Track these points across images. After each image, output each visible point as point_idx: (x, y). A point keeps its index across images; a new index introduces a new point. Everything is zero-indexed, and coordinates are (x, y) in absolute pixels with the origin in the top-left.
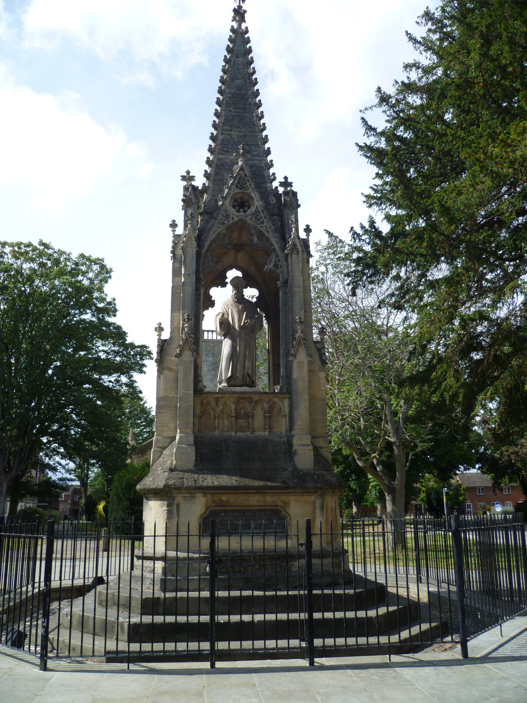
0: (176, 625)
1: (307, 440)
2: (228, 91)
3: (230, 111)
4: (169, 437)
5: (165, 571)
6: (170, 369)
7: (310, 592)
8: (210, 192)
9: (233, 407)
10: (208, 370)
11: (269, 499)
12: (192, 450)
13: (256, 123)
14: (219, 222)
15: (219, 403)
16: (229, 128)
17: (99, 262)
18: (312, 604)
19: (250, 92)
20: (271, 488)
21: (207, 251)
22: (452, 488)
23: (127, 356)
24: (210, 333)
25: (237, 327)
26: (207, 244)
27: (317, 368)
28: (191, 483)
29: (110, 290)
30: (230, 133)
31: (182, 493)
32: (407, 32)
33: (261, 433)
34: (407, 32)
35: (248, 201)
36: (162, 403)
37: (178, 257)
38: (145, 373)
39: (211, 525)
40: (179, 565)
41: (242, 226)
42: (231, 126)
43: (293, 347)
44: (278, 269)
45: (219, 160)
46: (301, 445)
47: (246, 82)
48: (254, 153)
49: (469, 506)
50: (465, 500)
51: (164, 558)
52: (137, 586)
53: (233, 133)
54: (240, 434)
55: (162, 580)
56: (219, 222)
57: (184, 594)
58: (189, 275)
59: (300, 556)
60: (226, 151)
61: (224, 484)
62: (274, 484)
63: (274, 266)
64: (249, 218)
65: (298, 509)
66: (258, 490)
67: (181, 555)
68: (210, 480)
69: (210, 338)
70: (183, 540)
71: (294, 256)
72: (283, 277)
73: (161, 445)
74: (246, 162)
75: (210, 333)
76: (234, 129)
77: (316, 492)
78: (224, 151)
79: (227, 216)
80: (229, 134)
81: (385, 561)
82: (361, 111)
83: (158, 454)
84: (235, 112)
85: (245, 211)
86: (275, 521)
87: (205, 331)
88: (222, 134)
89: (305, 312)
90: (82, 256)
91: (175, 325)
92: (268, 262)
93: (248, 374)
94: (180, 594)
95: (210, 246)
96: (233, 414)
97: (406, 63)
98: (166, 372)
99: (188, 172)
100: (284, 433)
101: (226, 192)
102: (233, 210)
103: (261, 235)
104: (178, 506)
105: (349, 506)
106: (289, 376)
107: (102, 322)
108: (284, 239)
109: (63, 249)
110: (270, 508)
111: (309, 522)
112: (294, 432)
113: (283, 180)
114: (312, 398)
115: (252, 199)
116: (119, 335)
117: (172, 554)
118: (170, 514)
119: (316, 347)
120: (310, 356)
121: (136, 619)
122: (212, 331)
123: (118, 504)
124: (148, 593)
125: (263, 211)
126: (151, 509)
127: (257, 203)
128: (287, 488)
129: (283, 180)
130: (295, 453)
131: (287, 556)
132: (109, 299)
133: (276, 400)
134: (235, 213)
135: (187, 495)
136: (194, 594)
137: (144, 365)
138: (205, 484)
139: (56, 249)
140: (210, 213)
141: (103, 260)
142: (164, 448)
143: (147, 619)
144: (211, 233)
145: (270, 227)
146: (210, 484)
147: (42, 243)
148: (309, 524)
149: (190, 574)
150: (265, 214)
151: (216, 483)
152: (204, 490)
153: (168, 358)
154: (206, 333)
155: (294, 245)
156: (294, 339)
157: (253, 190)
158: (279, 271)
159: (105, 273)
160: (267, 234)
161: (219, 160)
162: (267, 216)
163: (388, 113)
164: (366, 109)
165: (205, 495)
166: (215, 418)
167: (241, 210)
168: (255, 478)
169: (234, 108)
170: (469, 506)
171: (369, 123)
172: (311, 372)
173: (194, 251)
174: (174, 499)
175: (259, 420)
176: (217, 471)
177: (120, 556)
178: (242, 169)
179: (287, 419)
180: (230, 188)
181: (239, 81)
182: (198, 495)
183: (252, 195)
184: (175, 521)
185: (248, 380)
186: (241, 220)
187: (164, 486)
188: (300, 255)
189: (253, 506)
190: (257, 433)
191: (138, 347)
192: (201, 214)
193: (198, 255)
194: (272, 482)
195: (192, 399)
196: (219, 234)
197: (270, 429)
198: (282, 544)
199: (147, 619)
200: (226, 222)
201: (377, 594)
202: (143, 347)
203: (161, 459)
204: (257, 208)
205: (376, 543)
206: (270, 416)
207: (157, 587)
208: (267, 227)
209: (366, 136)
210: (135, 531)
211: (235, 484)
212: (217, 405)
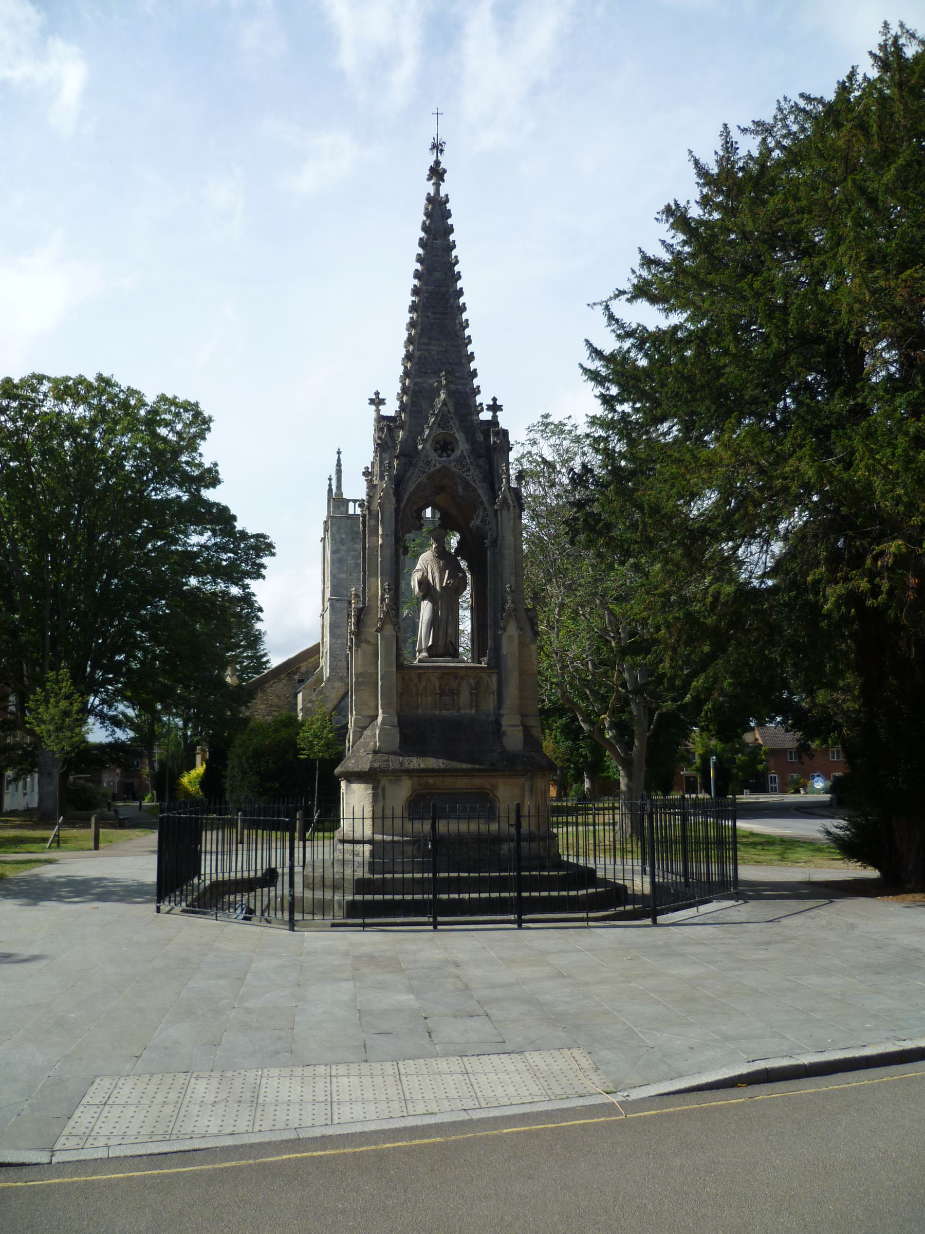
0: (393, 901)
1: (517, 720)
2: (424, 288)
4: (369, 717)
5: (372, 853)
6: (368, 642)
7: (519, 873)
8: (407, 427)
9: (437, 683)
11: (477, 782)
12: (396, 732)
14: (420, 470)
17: (193, 408)
18: (521, 884)
19: (451, 290)
20: (478, 770)
21: (406, 505)
22: (748, 750)
26: (406, 497)
27: (528, 639)
28: (397, 766)
29: (209, 452)
30: (428, 347)
32: (640, 249)
33: (468, 711)
34: (640, 249)
35: (451, 443)
36: (361, 679)
37: (374, 512)
38: (264, 577)
39: (417, 807)
41: (444, 472)
42: (430, 338)
43: (502, 619)
45: (416, 384)
46: (510, 726)
47: (446, 275)
48: (457, 374)
49: (773, 780)
50: (767, 770)
51: (371, 842)
53: (432, 347)
54: (445, 713)
55: (370, 863)
56: (420, 470)
59: (509, 839)
62: (481, 767)
64: (453, 464)
65: (507, 793)
67: (388, 838)
68: (416, 763)
70: (388, 823)
71: (505, 512)
74: (450, 394)
79: (428, 463)
81: (597, 842)
83: (358, 735)
84: (434, 318)
86: (483, 804)
87: (349, 501)
89: (516, 576)
90: (163, 398)
92: (475, 516)
93: (451, 643)
95: (409, 499)
96: (437, 691)
98: (364, 645)
99: (377, 394)
101: (427, 433)
102: (435, 454)
103: (467, 485)
104: (383, 789)
105: (579, 779)
106: (497, 649)
107: (196, 499)
108: (493, 489)
111: (518, 806)
112: (503, 711)
113: (491, 403)
114: (522, 673)
115: (457, 441)
116: (221, 519)
117: (378, 837)
119: (528, 616)
120: (521, 629)
121: (349, 898)
123: (242, 779)
124: (359, 874)
127: (463, 446)
128: (496, 771)
129: (491, 403)
130: (504, 734)
131: (496, 840)
132: (207, 465)
133: (483, 675)
137: (262, 566)
138: (411, 766)
139: (124, 387)
140: (409, 455)
142: (365, 728)
143: (358, 897)
146: (416, 767)
147: (100, 378)
148: (519, 808)
152: (410, 772)
154: (351, 504)
155: (505, 499)
156: (503, 610)
158: (487, 527)
159: (201, 422)
160: (473, 484)
163: (618, 332)
165: (411, 777)
166: (418, 695)
169: (433, 313)
170: (773, 780)
171: (595, 346)
172: (522, 645)
173: (393, 508)
174: (379, 782)
175: (464, 697)
176: (422, 754)
177: (270, 849)
178: (444, 403)
180: (431, 428)
182: (404, 778)
183: (457, 436)
184: (380, 804)
185: (451, 649)
186: (443, 467)
188: (511, 511)
190: (463, 712)
191: (253, 536)
192: (397, 457)
193: (397, 511)
195: (394, 677)
197: (477, 707)
198: (494, 827)
199: (358, 897)
201: (587, 876)
202: (258, 536)
203: (362, 740)
205: (607, 834)
206: (476, 693)
207: (366, 869)
208: (473, 476)
210: (329, 816)
211: (442, 766)
212: (420, 681)
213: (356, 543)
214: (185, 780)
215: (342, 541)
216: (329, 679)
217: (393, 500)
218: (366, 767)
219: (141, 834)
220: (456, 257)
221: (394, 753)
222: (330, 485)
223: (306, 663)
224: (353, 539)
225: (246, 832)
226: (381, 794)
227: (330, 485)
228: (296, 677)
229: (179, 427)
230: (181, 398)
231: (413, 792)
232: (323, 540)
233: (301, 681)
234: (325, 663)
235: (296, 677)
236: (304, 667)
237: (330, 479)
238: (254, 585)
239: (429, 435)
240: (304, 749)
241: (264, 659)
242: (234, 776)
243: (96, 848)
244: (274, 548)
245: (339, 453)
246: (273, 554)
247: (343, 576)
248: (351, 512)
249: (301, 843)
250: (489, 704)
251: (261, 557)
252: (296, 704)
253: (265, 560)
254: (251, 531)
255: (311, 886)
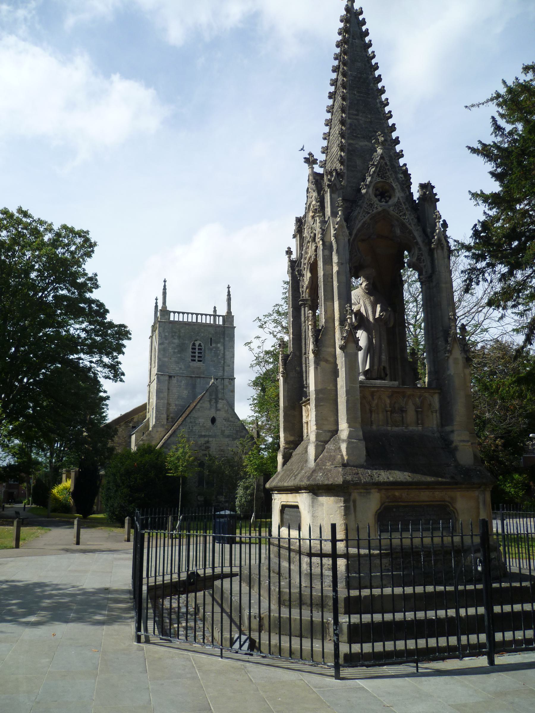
2: (349, 73)
3: (354, 94)
4: (329, 431)
6: (327, 361)
10: (174, 352)
11: (438, 495)
12: (362, 445)
13: (380, 109)
14: (364, 211)
15: (375, 397)
16: (355, 112)
17: (83, 234)
19: (371, 77)
20: (441, 483)
23: (104, 335)
24: (176, 314)
25: (371, 319)
28: (368, 480)
29: (90, 267)
30: (357, 117)
31: (357, 489)
36: (321, 396)
37: (327, 244)
38: (123, 353)
39: (386, 518)
40: (361, 562)
41: (384, 215)
44: (420, 263)
45: (350, 144)
47: (365, 65)
52: (317, 585)
53: (360, 118)
54: (396, 429)
57: (366, 592)
58: (342, 264)
60: (356, 137)
61: (399, 480)
62: (444, 480)
63: (417, 260)
64: (391, 208)
66: (428, 486)
67: (363, 552)
68: (384, 476)
69: (176, 319)
71: (439, 251)
72: (426, 272)
73: (322, 439)
75: (176, 314)
76: (361, 114)
77: (480, 487)
78: (353, 136)
79: (371, 205)
80: (356, 119)
82: (466, 107)
83: (321, 448)
84: (359, 96)
85: (387, 202)
87: (171, 312)
88: (349, 118)
90: (65, 227)
91: (329, 315)
94: (366, 592)
97: (526, 64)
98: (323, 364)
100: (435, 429)
103: (403, 226)
104: (354, 502)
109: (42, 219)
110: (439, 503)
115: (393, 189)
117: (353, 551)
118: (347, 512)
122: (210, 315)
123: (116, 491)
125: (404, 203)
126: (323, 505)
128: (456, 484)
131: (460, 551)
132: (90, 275)
134: (377, 202)
135: (362, 491)
136: (377, 592)
138: (381, 479)
140: (351, 202)
141: (87, 232)
142: (326, 442)
144: (357, 222)
145: (412, 219)
147: (20, 211)
149: (372, 571)
150: (407, 206)
151: (391, 479)
152: (379, 485)
153: (324, 349)
154: (172, 314)
157: (393, 180)
159: (88, 247)
160: (409, 226)
161: (350, 144)
162: (409, 208)
164: (473, 106)
165: (380, 490)
167: (383, 200)
168: (424, 474)
169: (358, 92)
173: (346, 240)
174: (350, 495)
175: (411, 415)
176: (388, 467)
178: (382, 157)
179: (438, 414)
180: (372, 176)
181: (359, 64)
182: (372, 491)
183: (394, 185)
186: (384, 210)
187: (344, 482)
189: (424, 502)
190: (411, 428)
191: (116, 326)
194: (442, 477)
196: (364, 223)
197: (422, 424)
200: (371, 211)
203: (325, 453)
204: (399, 199)
209: (494, 135)
211: (410, 479)
213: (175, 339)
214: (55, 491)
215: (166, 338)
216: (154, 426)
217: (347, 232)
218: (340, 480)
219: (43, 531)
220: (373, 52)
221: (361, 466)
222: (156, 306)
223: (137, 416)
224: (173, 336)
225: (217, 545)
226: (352, 507)
227: (156, 303)
228: (131, 425)
229: (73, 248)
230: (77, 229)
231: (382, 505)
232: (151, 337)
233: (134, 427)
234: (151, 417)
235: (131, 425)
236: (136, 418)
237: (156, 299)
238: (121, 358)
239: (370, 182)
240: (171, 469)
241: (104, 414)
242: (109, 488)
243: (17, 546)
244: (130, 334)
245: (165, 281)
246: (130, 339)
247: (166, 359)
248: (172, 319)
249: (170, 541)
250: (433, 421)
251: (123, 340)
252: (130, 442)
253: (125, 342)
254: (116, 322)
255: (287, 603)
